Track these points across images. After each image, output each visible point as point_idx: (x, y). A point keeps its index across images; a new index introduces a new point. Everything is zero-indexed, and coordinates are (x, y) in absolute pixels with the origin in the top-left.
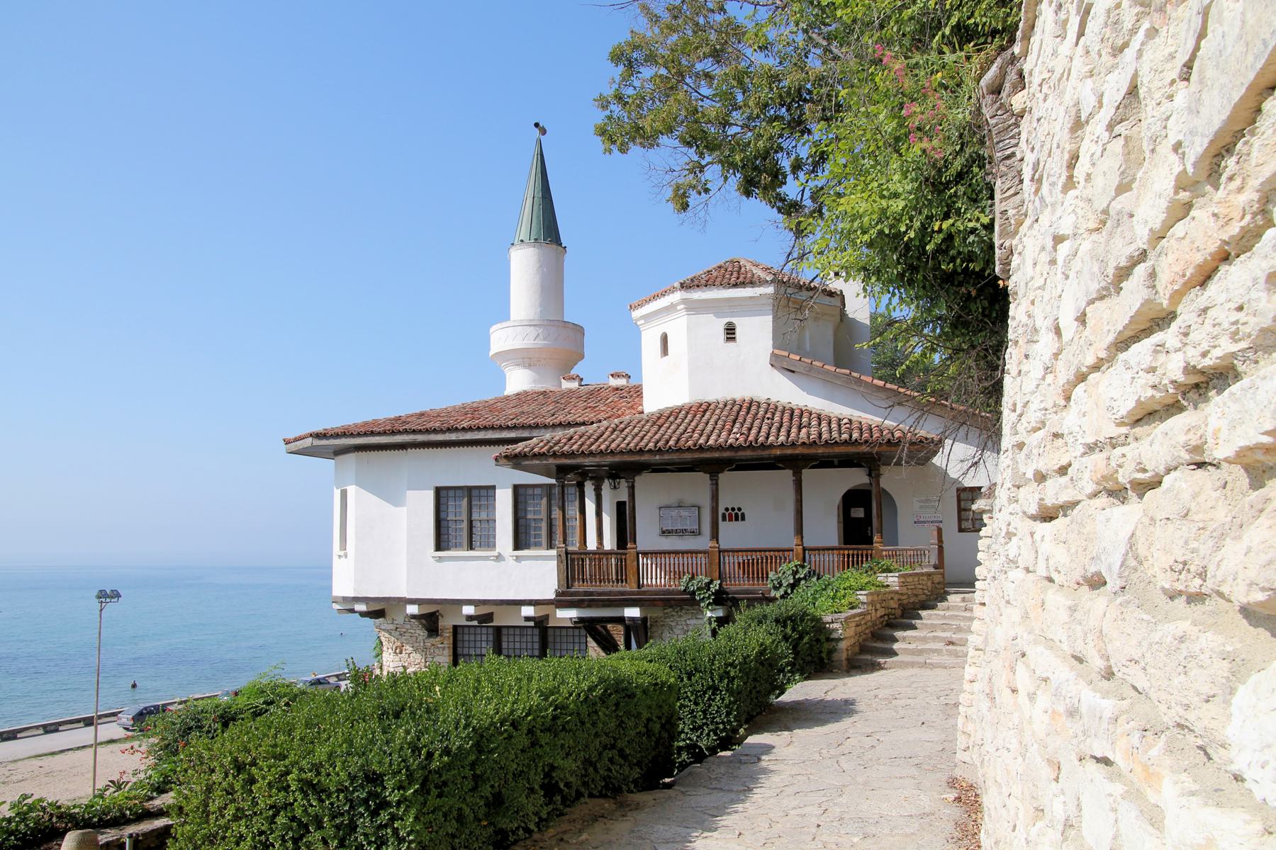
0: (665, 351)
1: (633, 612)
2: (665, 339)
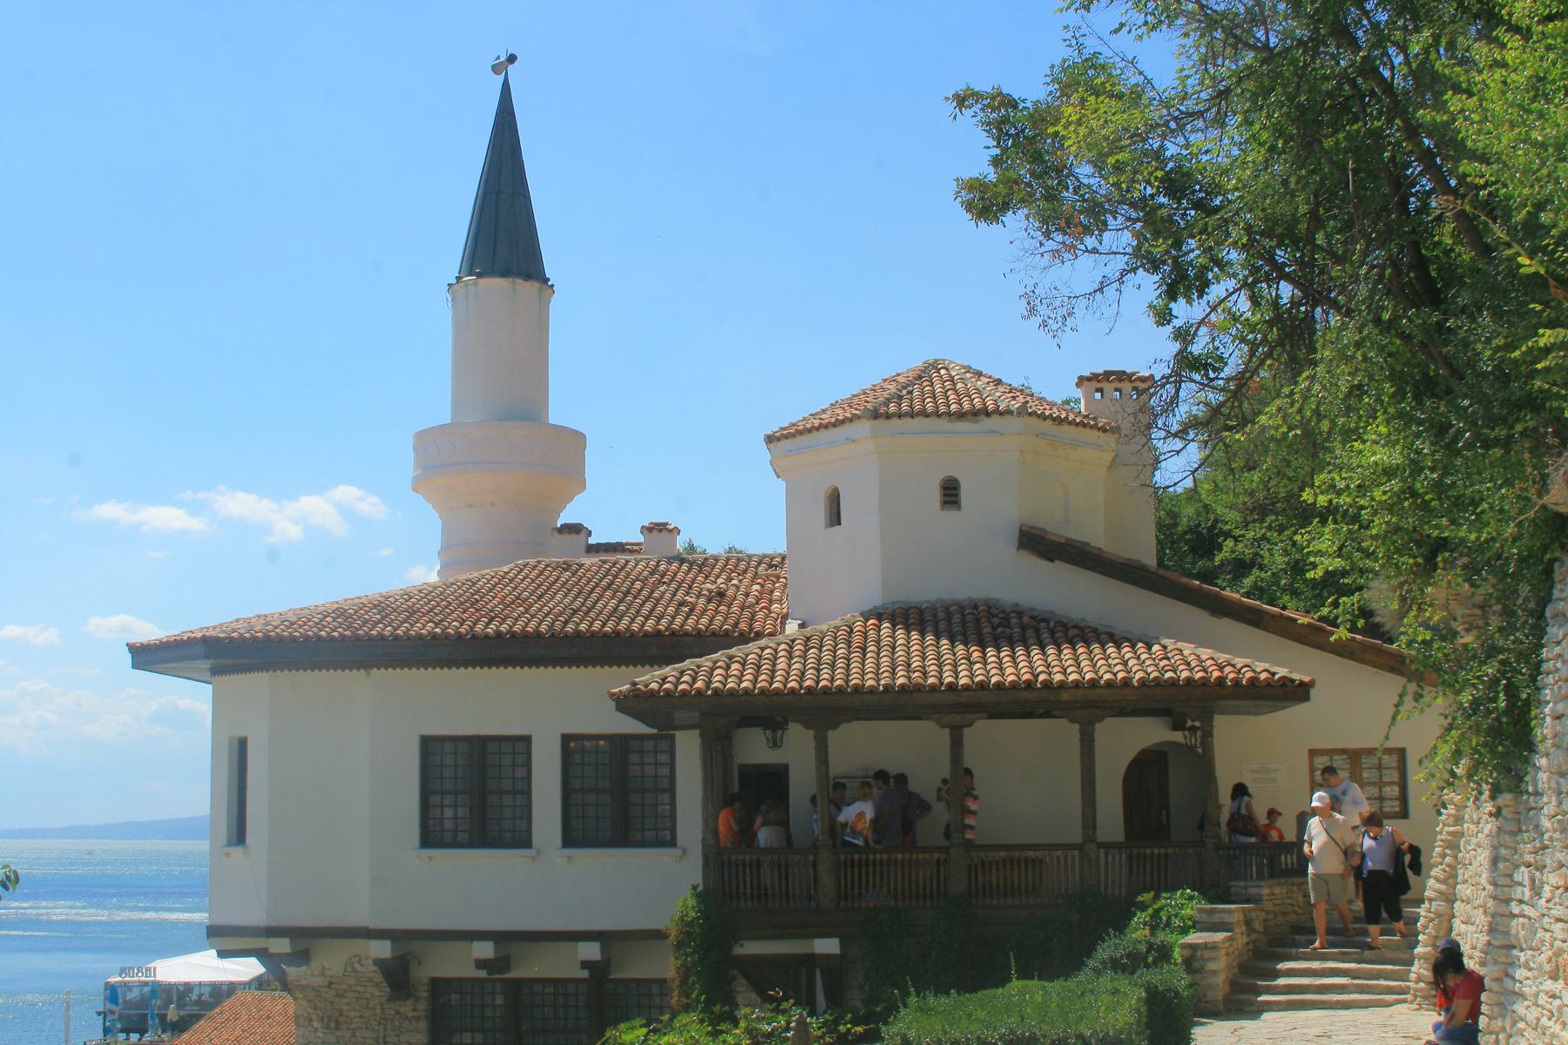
0: (835, 518)
1: (828, 946)
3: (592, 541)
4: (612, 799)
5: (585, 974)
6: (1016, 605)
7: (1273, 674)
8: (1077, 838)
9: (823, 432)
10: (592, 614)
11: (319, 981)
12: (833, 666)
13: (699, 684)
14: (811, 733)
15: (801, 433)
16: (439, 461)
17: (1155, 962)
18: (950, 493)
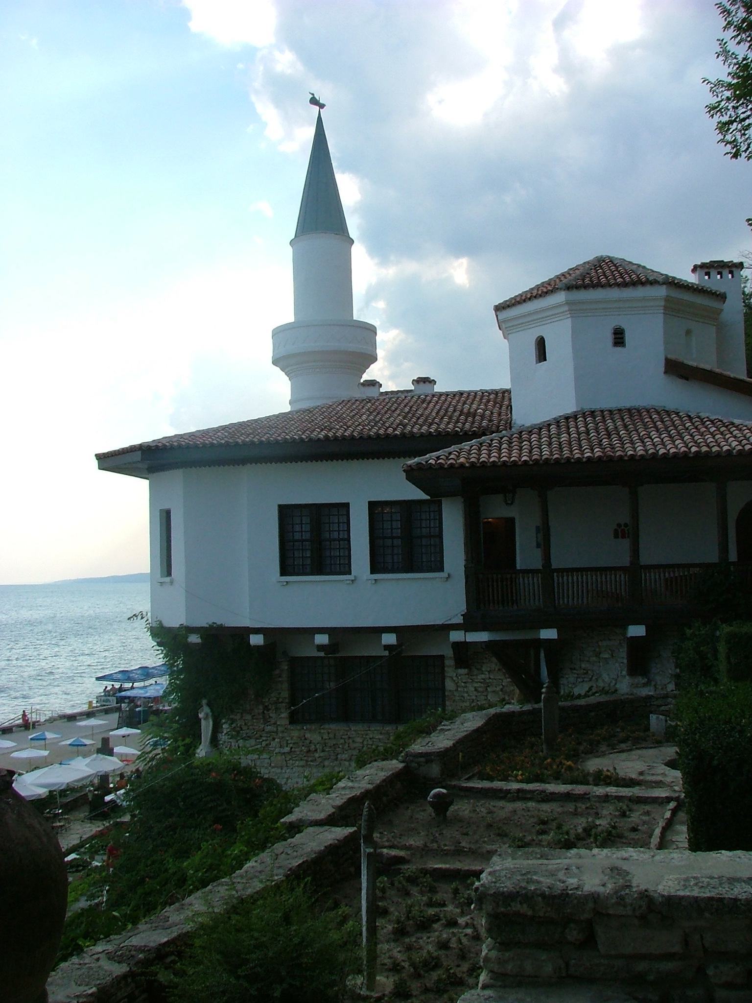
1: (549, 634)
2: (541, 344)
3: (382, 390)
4: (403, 544)
13: (462, 460)
17: (210, 771)
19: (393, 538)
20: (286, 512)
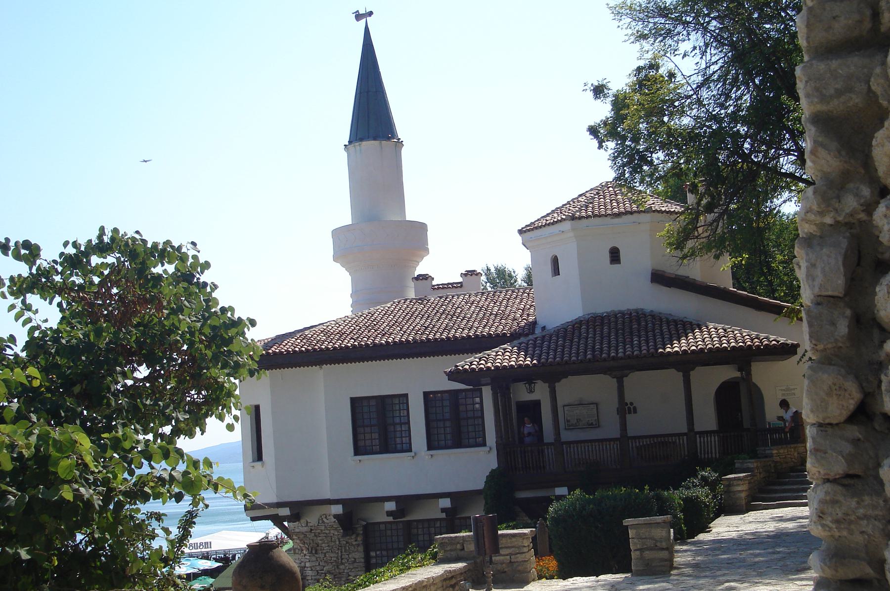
0: (556, 271)
3: (434, 283)
4: (451, 423)
5: (444, 515)
6: (652, 311)
7: (778, 342)
8: (685, 430)
9: (547, 228)
10: (435, 329)
11: (305, 529)
12: (555, 351)
14: (681, 374)
15: (536, 228)
16: (348, 246)
18: (615, 256)
19: (444, 420)
20: (356, 403)
